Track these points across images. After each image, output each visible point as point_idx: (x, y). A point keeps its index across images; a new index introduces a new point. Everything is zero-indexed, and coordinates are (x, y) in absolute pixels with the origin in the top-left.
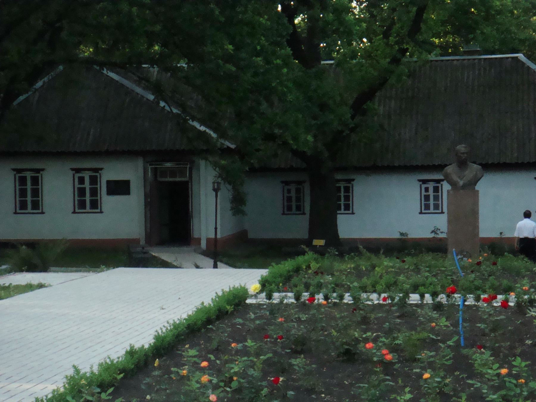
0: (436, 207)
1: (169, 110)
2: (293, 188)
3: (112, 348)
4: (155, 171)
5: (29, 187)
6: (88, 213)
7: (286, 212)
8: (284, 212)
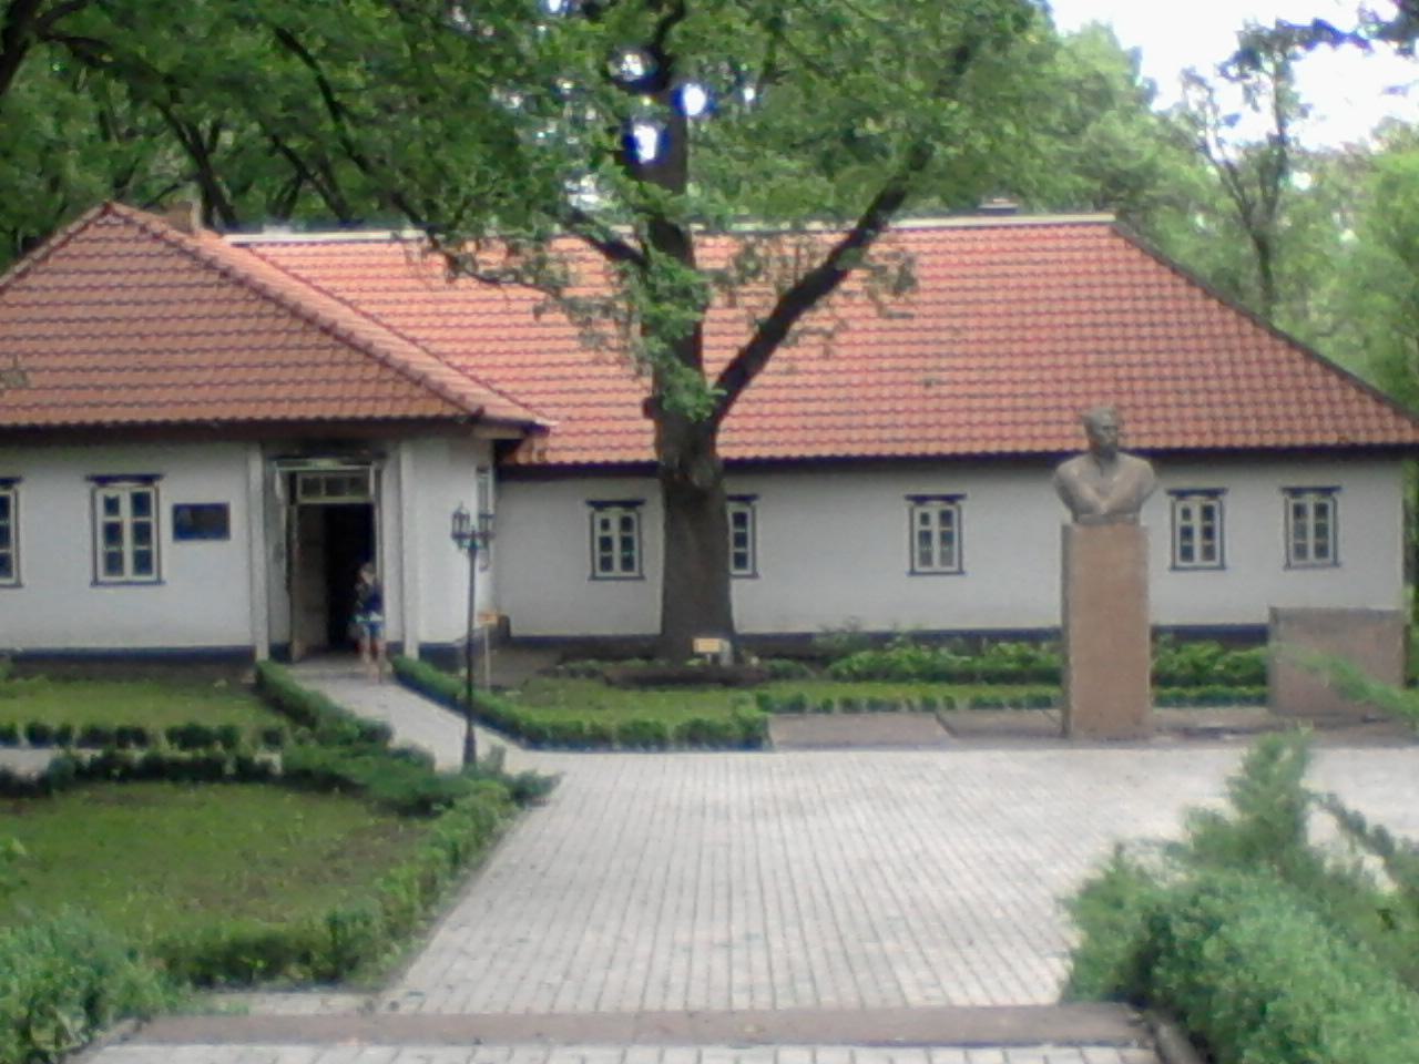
0: (1209, 553)
1: (1407, 340)
4: (291, 480)
6: (129, 583)
7: (102, 577)
8: (594, 571)
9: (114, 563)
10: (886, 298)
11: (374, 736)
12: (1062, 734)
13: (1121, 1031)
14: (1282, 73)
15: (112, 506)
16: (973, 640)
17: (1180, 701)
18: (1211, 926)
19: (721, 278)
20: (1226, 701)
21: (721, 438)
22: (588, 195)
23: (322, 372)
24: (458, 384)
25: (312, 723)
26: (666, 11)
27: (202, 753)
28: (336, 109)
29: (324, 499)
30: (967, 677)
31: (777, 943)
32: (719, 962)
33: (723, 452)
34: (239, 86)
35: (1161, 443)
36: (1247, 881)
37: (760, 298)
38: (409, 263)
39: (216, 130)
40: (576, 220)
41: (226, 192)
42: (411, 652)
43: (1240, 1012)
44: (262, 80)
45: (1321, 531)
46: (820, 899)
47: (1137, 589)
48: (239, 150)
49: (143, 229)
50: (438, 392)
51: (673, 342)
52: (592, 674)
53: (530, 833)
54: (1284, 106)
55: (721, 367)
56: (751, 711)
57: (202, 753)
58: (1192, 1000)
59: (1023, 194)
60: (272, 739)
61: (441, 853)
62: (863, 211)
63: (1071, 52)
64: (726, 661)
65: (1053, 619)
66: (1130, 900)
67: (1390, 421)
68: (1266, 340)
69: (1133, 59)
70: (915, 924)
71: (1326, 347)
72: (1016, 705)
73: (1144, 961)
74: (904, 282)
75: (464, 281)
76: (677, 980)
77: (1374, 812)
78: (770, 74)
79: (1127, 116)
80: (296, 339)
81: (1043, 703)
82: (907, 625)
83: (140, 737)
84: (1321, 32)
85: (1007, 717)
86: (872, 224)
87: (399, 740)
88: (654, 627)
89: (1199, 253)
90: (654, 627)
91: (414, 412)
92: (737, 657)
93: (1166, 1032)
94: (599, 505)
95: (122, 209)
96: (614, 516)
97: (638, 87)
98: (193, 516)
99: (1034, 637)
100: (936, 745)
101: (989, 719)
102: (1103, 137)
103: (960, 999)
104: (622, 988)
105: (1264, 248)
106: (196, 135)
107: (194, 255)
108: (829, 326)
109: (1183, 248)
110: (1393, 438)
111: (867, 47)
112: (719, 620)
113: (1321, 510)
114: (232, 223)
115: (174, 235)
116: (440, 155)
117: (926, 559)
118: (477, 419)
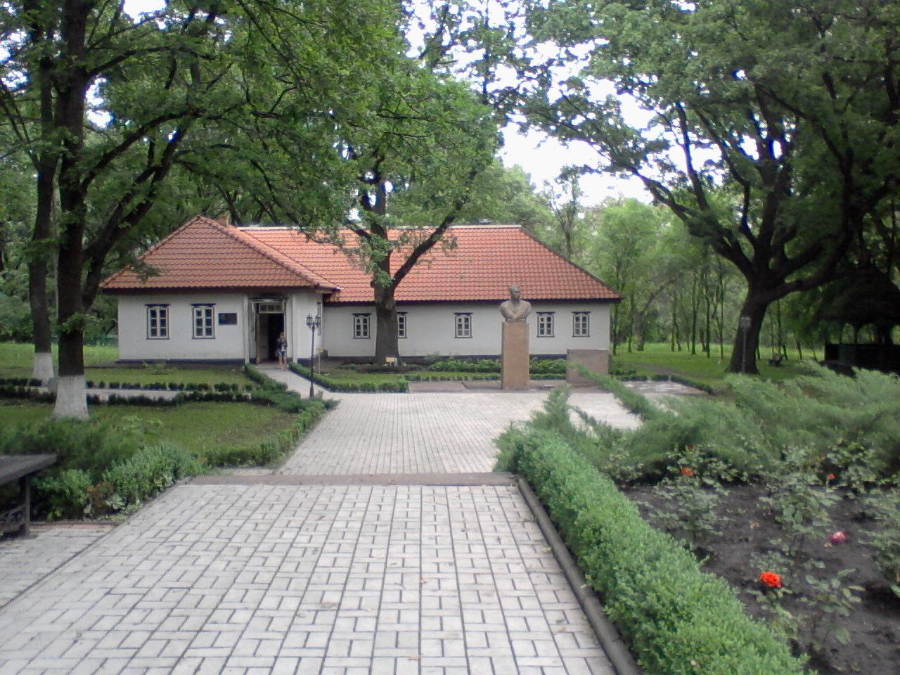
0: (549, 332)
2: (361, 318)
4: (257, 306)
5: (158, 318)
9: (199, 332)
10: (448, 250)
11: (282, 387)
12: (501, 388)
13: (507, 481)
14: (574, 182)
15: (199, 313)
16: (474, 359)
17: (539, 378)
18: (535, 448)
19: (396, 243)
20: (553, 378)
21: (395, 294)
22: (354, 214)
23: (267, 271)
24: (311, 276)
25: (262, 383)
26: (379, 158)
27: (226, 392)
28: (270, 187)
29: (268, 312)
30: (473, 370)
31: (406, 454)
32: (387, 459)
33: (396, 298)
34: (239, 179)
35: (535, 297)
36: (547, 433)
37: (408, 250)
38: (293, 237)
39: (236, 194)
40: (349, 223)
41: (239, 214)
42: (295, 361)
43: (542, 475)
44: (247, 176)
45: (584, 325)
46: (421, 439)
47: (526, 342)
48: (243, 200)
49: (210, 225)
50: (305, 278)
51: (378, 263)
52: (353, 368)
53: (330, 418)
54: (575, 194)
55: (395, 271)
56: (403, 380)
57: (226, 392)
58: (529, 471)
59: (493, 218)
60: (248, 388)
61: (299, 424)
62: (441, 222)
63: (509, 174)
64: (396, 365)
65: (498, 353)
66: (512, 439)
67: (606, 291)
68: (568, 265)
69: (529, 176)
70: (451, 448)
71: (588, 268)
72: (487, 379)
73: (516, 459)
74: (454, 245)
75: (311, 243)
76: (373, 465)
77: (590, 412)
78: (413, 179)
79: (527, 194)
80: (259, 261)
81: (495, 378)
82: (453, 354)
83: (206, 387)
84: (586, 169)
85: (484, 383)
86: (443, 227)
87: (290, 388)
88: (374, 354)
89: (548, 238)
90: (374, 354)
91: (297, 285)
92: (399, 363)
93: (521, 481)
94: (540, 313)
95: (204, 218)
96: (361, 318)
97: (370, 182)
99: (494, 358)
100: (461, 391)
101: (478, 383)
102: (518, 200)
103: (463, 471)
104: (357, 467)
105: (568, 237)
106: (229, 195)
107: (226, 233)
108: (430, 259)
109: (543, 237)
110: (607, 296)
111: (439, 168)
112: (395, 353)
113: (584, 319)
114: (241, 224)
115: (220, 227)
116: (304, 201)
117: (460, 333)
118: (317, 287)
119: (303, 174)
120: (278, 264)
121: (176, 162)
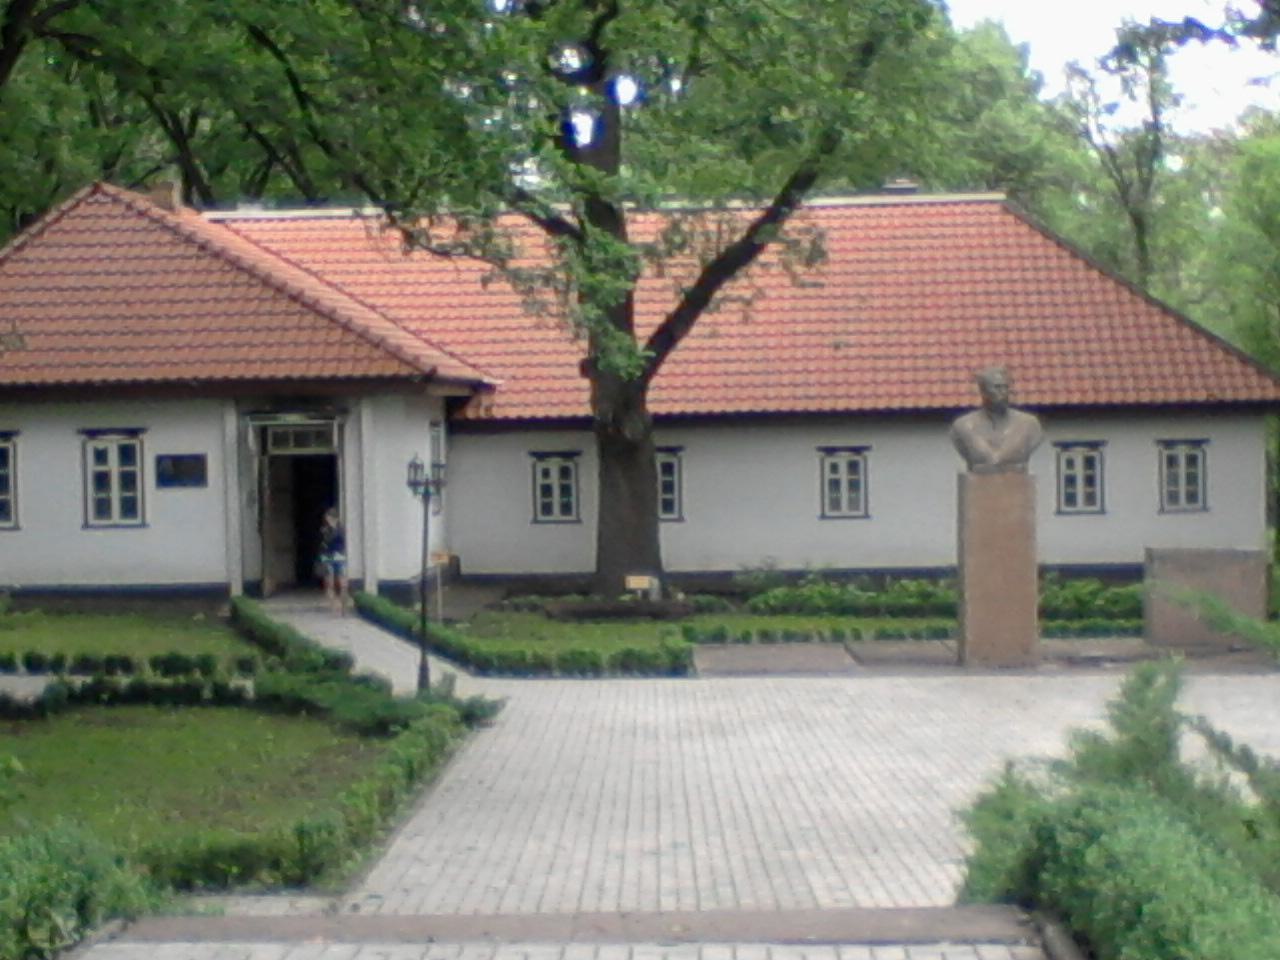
0: (1090, 499)
3: (627, 817)
4: (262, 433)
6: (116, 526)
7: (92, 521)
8: (535, 515)
9: (103, 508)
10: (799, 269)
11: (338, 664)
12: (958, 663)
13: (1011, 930)
14: (1156, 66)
15: (101, 456)
16: (878, 578)
17: (1064, 633)
18: (1092, 835)
19: (650, 251)
20: (1106, 632)
21: (650, 395)
22: (531, 176)
23: (291, 335)
24: (413, 346)
25: (281, 653)
26: (601, 10)
27: (182, 679)
28: (303, 99)
29: (293, 451)
30: (872, 611)
31: (701, 851)
32: (648, 868)
33: (652, 408)
34: (216, 77)
35: (1047, 400)
36: (1125, 795)
37: (686, 269)
39: (195, 117)
40: (520, 199)
41: (204, 173)
42: (371, 588)
44: (237, 72)
45: (1192, 479)
46: (740, 811)
47: (1025, 531)
48: (215, 135)
49: (129, 207)
50: (395, 354)
51: (607, 308)
52: (534, 608)
53: (478, 752)
54: (1158, 96)
55: (650, 331)
56: (677, 642)
57: (182, 679)
58: (1075, 902)
59: (922, 175)
60: (245, 667)
61: (398, 770)
62: (778, 190)
63: (966, 47)
64: (655, 597)
65: (950, 559)
66: (1020, 812)
67: (1254, 380)
68: (1142, 306)
69: (1022, 53)
71: (1196, 313)
72: (916, 636)
73: (1032, 867)
74: (816, 255)
75: (418, 254)
76: (611, 884)
77: (1240, 733)
78: (695, 67)
79: (1017, 104)
80: (267, 306)
81: (941, 634)
82: (818, 564)
83: (126, 665)
84: (1191, 29)
85: (908, 647)
86: (787, 202)
87: (360, 668)
88: (590, 566)
89: (1082, 228)
90: (590, 566)
91: (373, 372)
92: (665, 593)
93: (1052, 931)
94: (541, 456)
95: (110, 188)
96: (554, 465)
97: (575, 78)
98: (174, 465)
99: (933, 574)
100: (845, 672)
101: (892, 648)
102: (995, 123)
103: (866, 902)
104: (561, 891)
105: (1140, 224)
106: (177, 121)
107: (175, 230)
108: (748, 294)
109: (1067, 224)
110: (1257, 395)
111: (782, 42)
112: (648, 560)
113: (1192, 461)
114: (209, 201)
115: (157, 212)
116: (397, 140)
117: (836, 504)
118: (431, 378)
119: (396, 63)
120: (320, 313)
121: (41, 34)
